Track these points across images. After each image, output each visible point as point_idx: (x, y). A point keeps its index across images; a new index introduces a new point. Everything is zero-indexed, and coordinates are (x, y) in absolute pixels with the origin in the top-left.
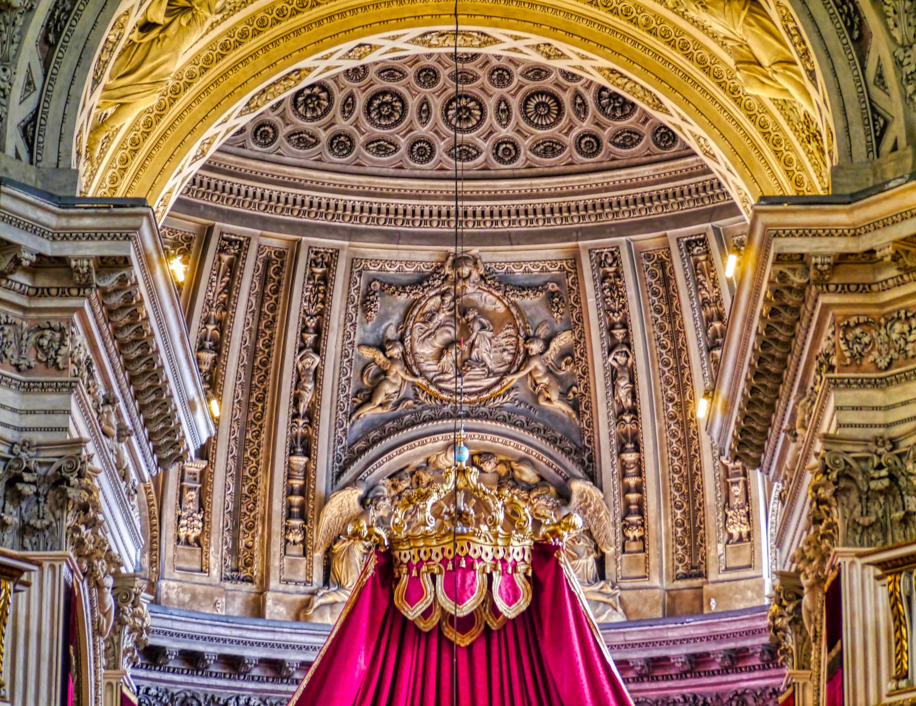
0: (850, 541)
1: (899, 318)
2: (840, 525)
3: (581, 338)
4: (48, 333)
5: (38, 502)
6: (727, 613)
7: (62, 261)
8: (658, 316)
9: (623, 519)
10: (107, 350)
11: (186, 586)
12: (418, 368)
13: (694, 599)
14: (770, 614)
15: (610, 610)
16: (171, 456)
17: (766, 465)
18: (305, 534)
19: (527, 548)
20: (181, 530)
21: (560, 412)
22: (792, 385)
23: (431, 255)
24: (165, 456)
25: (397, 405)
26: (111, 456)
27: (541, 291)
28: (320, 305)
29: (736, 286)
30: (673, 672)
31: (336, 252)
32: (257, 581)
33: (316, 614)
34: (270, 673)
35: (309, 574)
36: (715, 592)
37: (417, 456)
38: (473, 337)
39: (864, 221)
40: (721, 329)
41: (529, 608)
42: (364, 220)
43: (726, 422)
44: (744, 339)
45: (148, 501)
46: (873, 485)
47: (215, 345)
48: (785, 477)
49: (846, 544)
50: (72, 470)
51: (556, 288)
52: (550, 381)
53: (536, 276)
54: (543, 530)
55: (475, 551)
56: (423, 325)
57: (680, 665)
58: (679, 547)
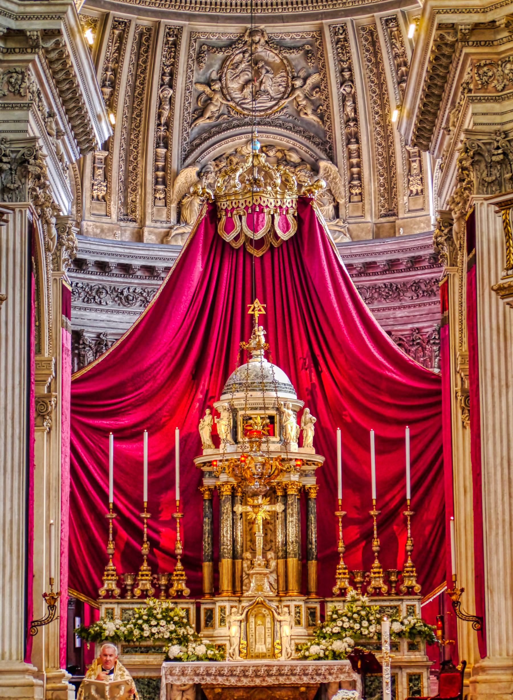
0: (481, 191)
1: (509, 61)
2: (475, 182)
3: (325, 77)
4: (14, 75)
5: (11, 174)
6: (409, 236)
7: (21, 32)
8: (369, 64)
9: (350, 183)
10: (49, 85)
11: (98, 224)
12: (230, 96)
13: (390, 229)
14: (433, 236)
15: (342, 235)
16: (88, 147)
17: (432, 149)
18: (166, 194)
19: (294, 200)
20: (94, 192)
21: (313, 121)
22: (447, 102)
23: (236, 29)
24: (84, 147)
25: (218, 118)
26: (53, 147)
27: (301, 50)
28: (172, 60)
29: (414, 45)
30: (379, 270)
31: (181, 29)
32: (139, 221)
33: (173, 240)
34: (147, 274)
35: (168, 216)
36: (402, 225)
37: (230, 148)
38: (262, 77)
39: (489, 4)
40: (406, 71)
41: (295, 234)
42: (197, 9)
43: (409, 124)
44: (419, 75)
45: (75, 175)
46: (494, 158)
47: (111, 84)
48: (443, 155)
49: (478, 193)
50: (30, 155)
51: (310, 48)
52: (307, 103)
53: (299, 41)
54: (303, 189)
55: (264, 202)
56: (232, 71)
57: (382, 266)
58: (382, 199)
